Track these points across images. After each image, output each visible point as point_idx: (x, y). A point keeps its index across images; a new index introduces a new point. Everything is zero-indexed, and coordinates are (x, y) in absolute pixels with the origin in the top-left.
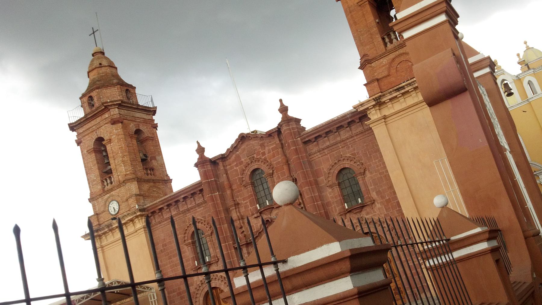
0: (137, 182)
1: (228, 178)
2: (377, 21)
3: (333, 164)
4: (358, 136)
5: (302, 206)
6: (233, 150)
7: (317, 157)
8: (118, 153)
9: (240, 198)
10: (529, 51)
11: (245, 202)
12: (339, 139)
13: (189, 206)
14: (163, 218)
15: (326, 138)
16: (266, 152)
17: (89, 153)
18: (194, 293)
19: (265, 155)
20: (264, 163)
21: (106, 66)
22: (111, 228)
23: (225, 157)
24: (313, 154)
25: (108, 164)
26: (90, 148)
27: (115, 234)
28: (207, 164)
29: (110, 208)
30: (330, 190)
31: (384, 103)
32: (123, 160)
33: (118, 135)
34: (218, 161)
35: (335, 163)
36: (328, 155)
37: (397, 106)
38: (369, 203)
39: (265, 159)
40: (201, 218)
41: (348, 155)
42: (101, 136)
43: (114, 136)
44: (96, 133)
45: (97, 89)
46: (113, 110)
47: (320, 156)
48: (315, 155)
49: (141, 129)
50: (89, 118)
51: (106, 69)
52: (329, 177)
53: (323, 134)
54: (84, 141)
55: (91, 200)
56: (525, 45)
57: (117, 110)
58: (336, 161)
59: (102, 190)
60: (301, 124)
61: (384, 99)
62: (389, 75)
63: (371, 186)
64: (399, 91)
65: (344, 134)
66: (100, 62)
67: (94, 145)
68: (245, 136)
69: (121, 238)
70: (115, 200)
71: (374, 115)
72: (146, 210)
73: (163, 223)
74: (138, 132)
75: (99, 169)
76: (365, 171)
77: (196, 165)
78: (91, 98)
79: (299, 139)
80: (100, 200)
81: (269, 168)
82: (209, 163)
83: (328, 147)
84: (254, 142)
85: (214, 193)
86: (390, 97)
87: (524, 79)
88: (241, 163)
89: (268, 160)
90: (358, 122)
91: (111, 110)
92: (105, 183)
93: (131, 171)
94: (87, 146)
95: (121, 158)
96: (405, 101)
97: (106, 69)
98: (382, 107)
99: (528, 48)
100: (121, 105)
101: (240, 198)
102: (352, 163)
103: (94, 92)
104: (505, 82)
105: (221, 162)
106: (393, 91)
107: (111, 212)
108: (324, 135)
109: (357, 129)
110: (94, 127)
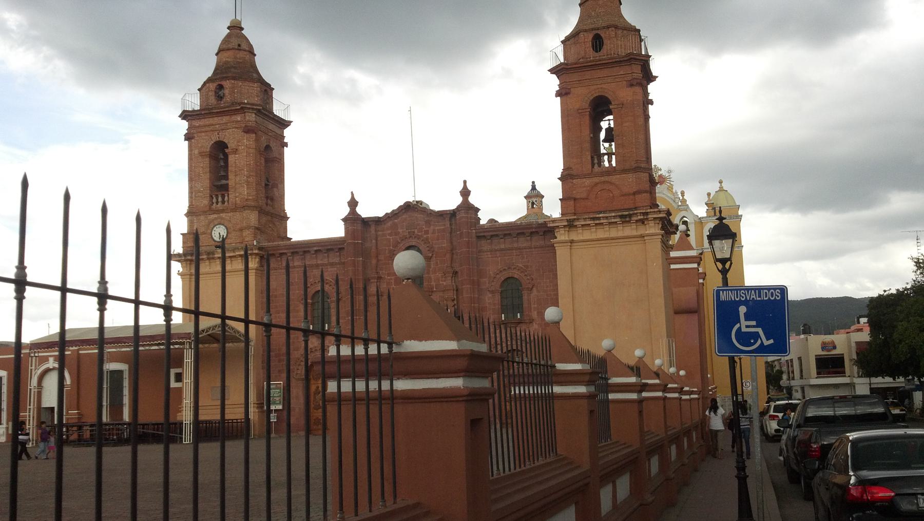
0: (259, 212)
1: (377, 243)
2: (592, 135)
3: (501, 270)
4: (537, 250)
5: (455, 302)
6: (392, 217)
7: (486, 256)
8: (243, 170)
9: (384, 272)
10: (721, 193)
11: (389, 278)
12: (515, 245)
13: (319, 262)
14: (281, 265)
15: (503, 240)
16: (430, 232)
17: (201, 156)
18: (299, 359)
19: (428, 234)
20: (425, 243)
21: (245, 50)
22: (211, 256)
23: (380, 221)
24: (483, 252)
25: (226, 177)
26: (205, 150)
27: (213, 264)
28: (358, 222)
29: (213, 232)
30: (490, 295)
31: (576, 226)
32: (247, 180)
33: (248, 147)
34: (370, 223)
35: (505, 269)
36: (499, 258)
37: (587, 235)
38: (527, 321)
39: (427, 239)
40: (331, 280)
41: (521, 265)
42: (224, 141)
43: (243, 148)
44: (218, 134)
45: (232, 79)
46: (250, 114)
47: (490, 256)
48: (485, 254)
49: (271, 145)
50: (214, 112)
51: (245, 55)
52: (493, 281)
53: (501, 235)
54: (198, 138)
55: (188, 215)
56: (719, 184)
57: (254, 115)
58: (506, 268)
59: (208, 207)
60: (478, 214)
61: (577, 223)
62: (587, 199)
63: (534, 304)
64: (594, 220)
65: (523, 242)
66: (239, 43)
67: (210, 148)
68: (412, 206)
69: (221, 272)
70: (223, 225)
71: (562, 236)
72: (264, 250)
73: (280, 271)
74: (268, 147)
75: (210, 179)
76: (532, 287)
77: (345, 220)
78: (221, 87)
79: (474, 231)
80: (202, 217)
81: (429, 250)
82: (360, 222)
83: (502, 250)
84: (419, 215)
85: (357, 258)
86: (583, 223)
87: (707, 224)
88: (397, 234)
89: (430, 241)
90: (541, 235)
91: (247, 114)
92: (214, 200)
93: (254, 197)
94: (200, 145)
95: (245, 177)
96: (596, 232)
97: (245, 55)
98: (571, 229)
99: (721, 189)
100: (259, 112)
101: (384, 272)
102: (522, 275)
103: (228, 81)
104: (685, 219)
105: (374, 225)
106: (588, 218)
107: (213, 236)
108: (502, 236)
109: (537, 241)
110: (217, 126)
